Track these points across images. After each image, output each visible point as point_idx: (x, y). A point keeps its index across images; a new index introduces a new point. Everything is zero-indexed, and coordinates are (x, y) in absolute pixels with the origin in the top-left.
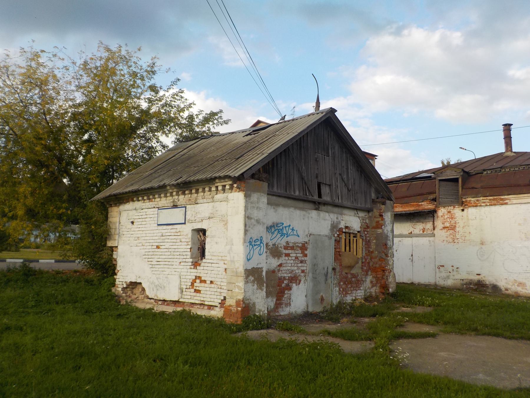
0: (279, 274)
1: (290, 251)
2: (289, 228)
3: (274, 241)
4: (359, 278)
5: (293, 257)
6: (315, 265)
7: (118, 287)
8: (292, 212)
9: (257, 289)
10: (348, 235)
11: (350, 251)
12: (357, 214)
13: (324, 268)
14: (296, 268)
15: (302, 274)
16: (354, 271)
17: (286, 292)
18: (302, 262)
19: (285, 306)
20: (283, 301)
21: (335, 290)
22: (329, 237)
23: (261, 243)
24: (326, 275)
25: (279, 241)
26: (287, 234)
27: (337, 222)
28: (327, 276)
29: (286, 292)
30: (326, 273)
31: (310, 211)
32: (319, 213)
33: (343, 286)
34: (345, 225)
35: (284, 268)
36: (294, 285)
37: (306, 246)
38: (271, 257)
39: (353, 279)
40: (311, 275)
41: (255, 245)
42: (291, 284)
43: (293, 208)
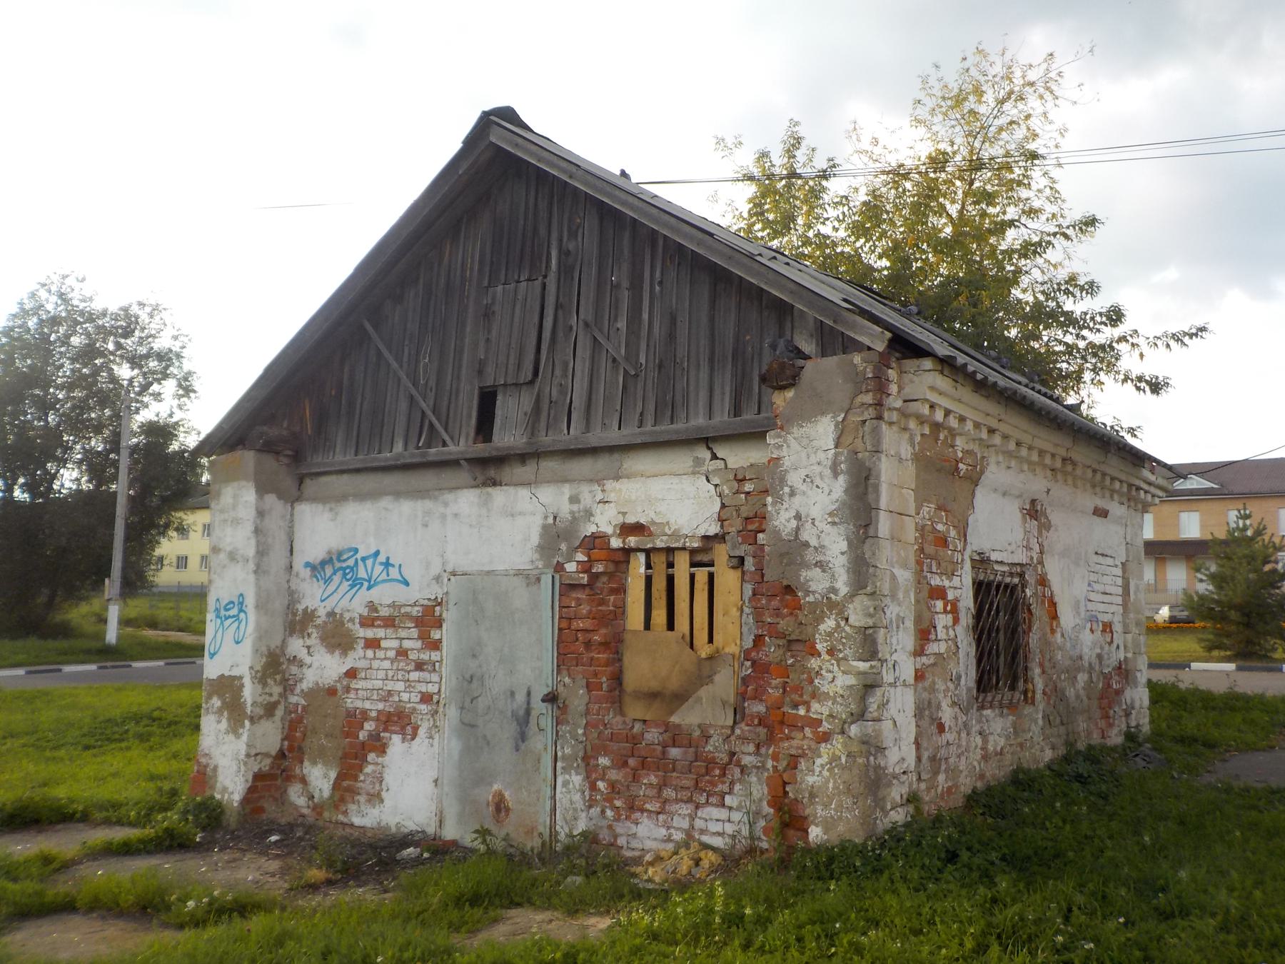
0: (349, 701)
1: (380, 633)
2: (374, 564)
3: (329, 605)
4: (709, 748)
5: (391, 649)
6: (470, 683)
7: (1137, 726)
8: (386, 509)
9: (227, 732)
10: (659, 561)
11: (671, 626)
12: (714, 457)
13: (513, 694)
14: (400, 686)
15: (423, 707)
16: (687, 717)
17: (371, 757)
18: (420, 666)
19: (369, 801)
20: (361, 784)
21: (565, 784)
22: (527, 577)
23: (241, 610)
24: (524, 720)
25: (344, 603)
26: (369, 581)
27: (572, 513)
28: (527, 722)
29: (371, 757)
30: (522, 712)
31: (449, 497)
32: (488, 494)
33: (613, 775)
34: (620, 519)
35: (368, 684)
36: (396, 739)
37: (437, 614)
38: (323, 650)
39: (674, 752)
40: (453, 712)
41: (227, 618)
42: (387, 735)
43: (389, 498)
